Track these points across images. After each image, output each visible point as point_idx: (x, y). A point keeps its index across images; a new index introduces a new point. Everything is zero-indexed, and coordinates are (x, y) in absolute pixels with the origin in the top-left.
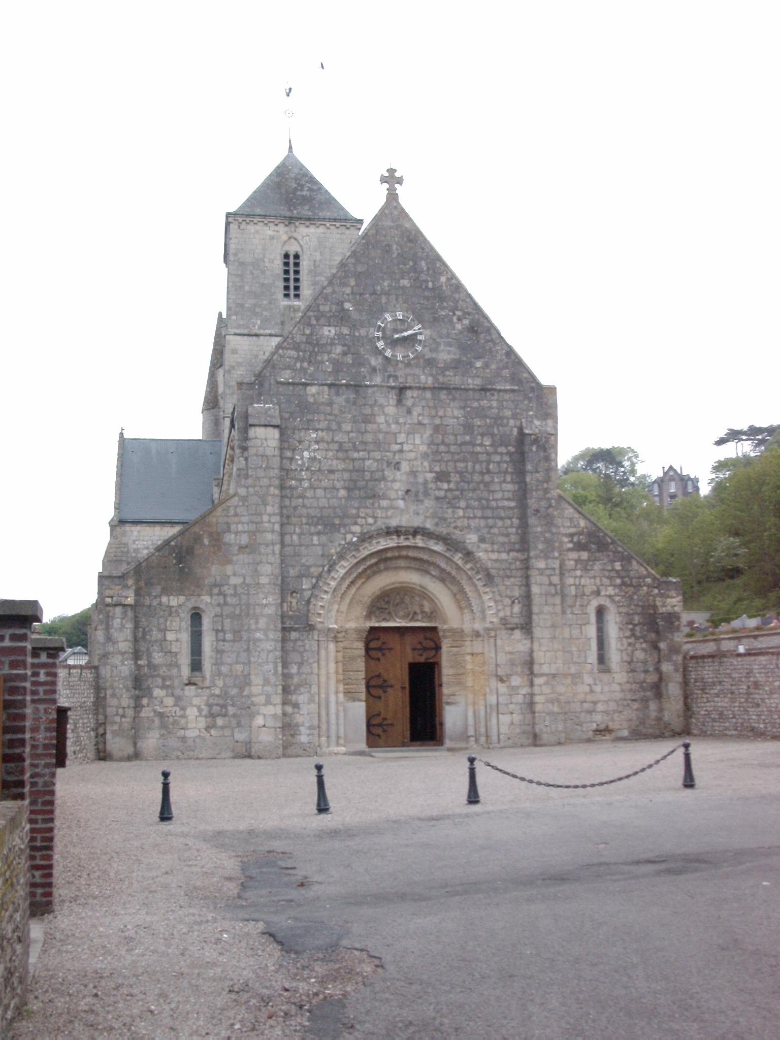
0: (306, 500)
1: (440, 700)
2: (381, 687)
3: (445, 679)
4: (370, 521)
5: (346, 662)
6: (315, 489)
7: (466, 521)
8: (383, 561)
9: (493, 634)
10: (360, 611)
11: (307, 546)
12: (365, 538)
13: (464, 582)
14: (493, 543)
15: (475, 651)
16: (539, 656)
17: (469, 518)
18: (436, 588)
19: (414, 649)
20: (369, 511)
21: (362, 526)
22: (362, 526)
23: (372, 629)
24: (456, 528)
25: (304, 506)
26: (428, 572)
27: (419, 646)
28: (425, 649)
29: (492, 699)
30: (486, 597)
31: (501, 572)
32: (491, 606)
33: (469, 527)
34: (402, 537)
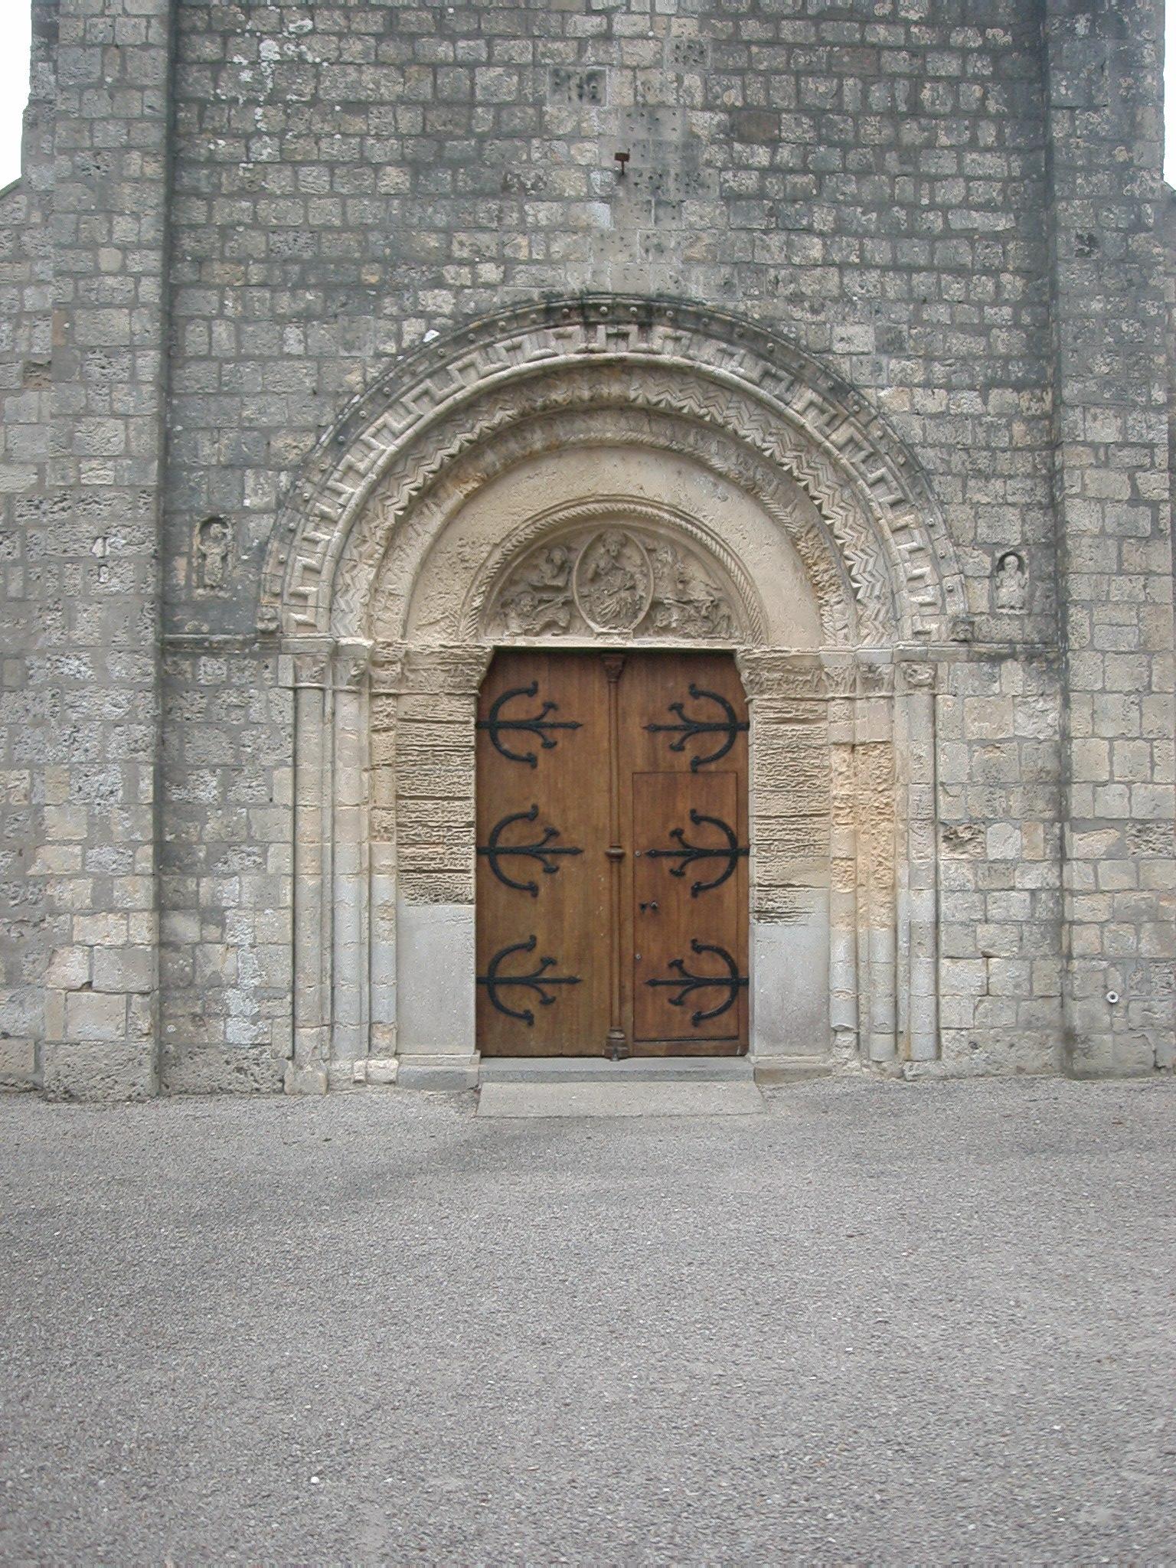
0: (263, 204)
2: (534, 853)
4: (490, 272)
8: (535, 417)
9: (924, 674)
10: (456, 590)
11: (263, 360)
12: (471, 332)
14: (929, 359)
16: (1090, 755)
17: (843, 267)
18: (748, 540)
19: (653, 729)
21: (458, 290)
22: (458, 290)
23: (502, 656)
24: (796, 299)
28: (693, 728)
29: (919, 906)
31: (957, 459)
32: (918, 579)
33: (844, 297)
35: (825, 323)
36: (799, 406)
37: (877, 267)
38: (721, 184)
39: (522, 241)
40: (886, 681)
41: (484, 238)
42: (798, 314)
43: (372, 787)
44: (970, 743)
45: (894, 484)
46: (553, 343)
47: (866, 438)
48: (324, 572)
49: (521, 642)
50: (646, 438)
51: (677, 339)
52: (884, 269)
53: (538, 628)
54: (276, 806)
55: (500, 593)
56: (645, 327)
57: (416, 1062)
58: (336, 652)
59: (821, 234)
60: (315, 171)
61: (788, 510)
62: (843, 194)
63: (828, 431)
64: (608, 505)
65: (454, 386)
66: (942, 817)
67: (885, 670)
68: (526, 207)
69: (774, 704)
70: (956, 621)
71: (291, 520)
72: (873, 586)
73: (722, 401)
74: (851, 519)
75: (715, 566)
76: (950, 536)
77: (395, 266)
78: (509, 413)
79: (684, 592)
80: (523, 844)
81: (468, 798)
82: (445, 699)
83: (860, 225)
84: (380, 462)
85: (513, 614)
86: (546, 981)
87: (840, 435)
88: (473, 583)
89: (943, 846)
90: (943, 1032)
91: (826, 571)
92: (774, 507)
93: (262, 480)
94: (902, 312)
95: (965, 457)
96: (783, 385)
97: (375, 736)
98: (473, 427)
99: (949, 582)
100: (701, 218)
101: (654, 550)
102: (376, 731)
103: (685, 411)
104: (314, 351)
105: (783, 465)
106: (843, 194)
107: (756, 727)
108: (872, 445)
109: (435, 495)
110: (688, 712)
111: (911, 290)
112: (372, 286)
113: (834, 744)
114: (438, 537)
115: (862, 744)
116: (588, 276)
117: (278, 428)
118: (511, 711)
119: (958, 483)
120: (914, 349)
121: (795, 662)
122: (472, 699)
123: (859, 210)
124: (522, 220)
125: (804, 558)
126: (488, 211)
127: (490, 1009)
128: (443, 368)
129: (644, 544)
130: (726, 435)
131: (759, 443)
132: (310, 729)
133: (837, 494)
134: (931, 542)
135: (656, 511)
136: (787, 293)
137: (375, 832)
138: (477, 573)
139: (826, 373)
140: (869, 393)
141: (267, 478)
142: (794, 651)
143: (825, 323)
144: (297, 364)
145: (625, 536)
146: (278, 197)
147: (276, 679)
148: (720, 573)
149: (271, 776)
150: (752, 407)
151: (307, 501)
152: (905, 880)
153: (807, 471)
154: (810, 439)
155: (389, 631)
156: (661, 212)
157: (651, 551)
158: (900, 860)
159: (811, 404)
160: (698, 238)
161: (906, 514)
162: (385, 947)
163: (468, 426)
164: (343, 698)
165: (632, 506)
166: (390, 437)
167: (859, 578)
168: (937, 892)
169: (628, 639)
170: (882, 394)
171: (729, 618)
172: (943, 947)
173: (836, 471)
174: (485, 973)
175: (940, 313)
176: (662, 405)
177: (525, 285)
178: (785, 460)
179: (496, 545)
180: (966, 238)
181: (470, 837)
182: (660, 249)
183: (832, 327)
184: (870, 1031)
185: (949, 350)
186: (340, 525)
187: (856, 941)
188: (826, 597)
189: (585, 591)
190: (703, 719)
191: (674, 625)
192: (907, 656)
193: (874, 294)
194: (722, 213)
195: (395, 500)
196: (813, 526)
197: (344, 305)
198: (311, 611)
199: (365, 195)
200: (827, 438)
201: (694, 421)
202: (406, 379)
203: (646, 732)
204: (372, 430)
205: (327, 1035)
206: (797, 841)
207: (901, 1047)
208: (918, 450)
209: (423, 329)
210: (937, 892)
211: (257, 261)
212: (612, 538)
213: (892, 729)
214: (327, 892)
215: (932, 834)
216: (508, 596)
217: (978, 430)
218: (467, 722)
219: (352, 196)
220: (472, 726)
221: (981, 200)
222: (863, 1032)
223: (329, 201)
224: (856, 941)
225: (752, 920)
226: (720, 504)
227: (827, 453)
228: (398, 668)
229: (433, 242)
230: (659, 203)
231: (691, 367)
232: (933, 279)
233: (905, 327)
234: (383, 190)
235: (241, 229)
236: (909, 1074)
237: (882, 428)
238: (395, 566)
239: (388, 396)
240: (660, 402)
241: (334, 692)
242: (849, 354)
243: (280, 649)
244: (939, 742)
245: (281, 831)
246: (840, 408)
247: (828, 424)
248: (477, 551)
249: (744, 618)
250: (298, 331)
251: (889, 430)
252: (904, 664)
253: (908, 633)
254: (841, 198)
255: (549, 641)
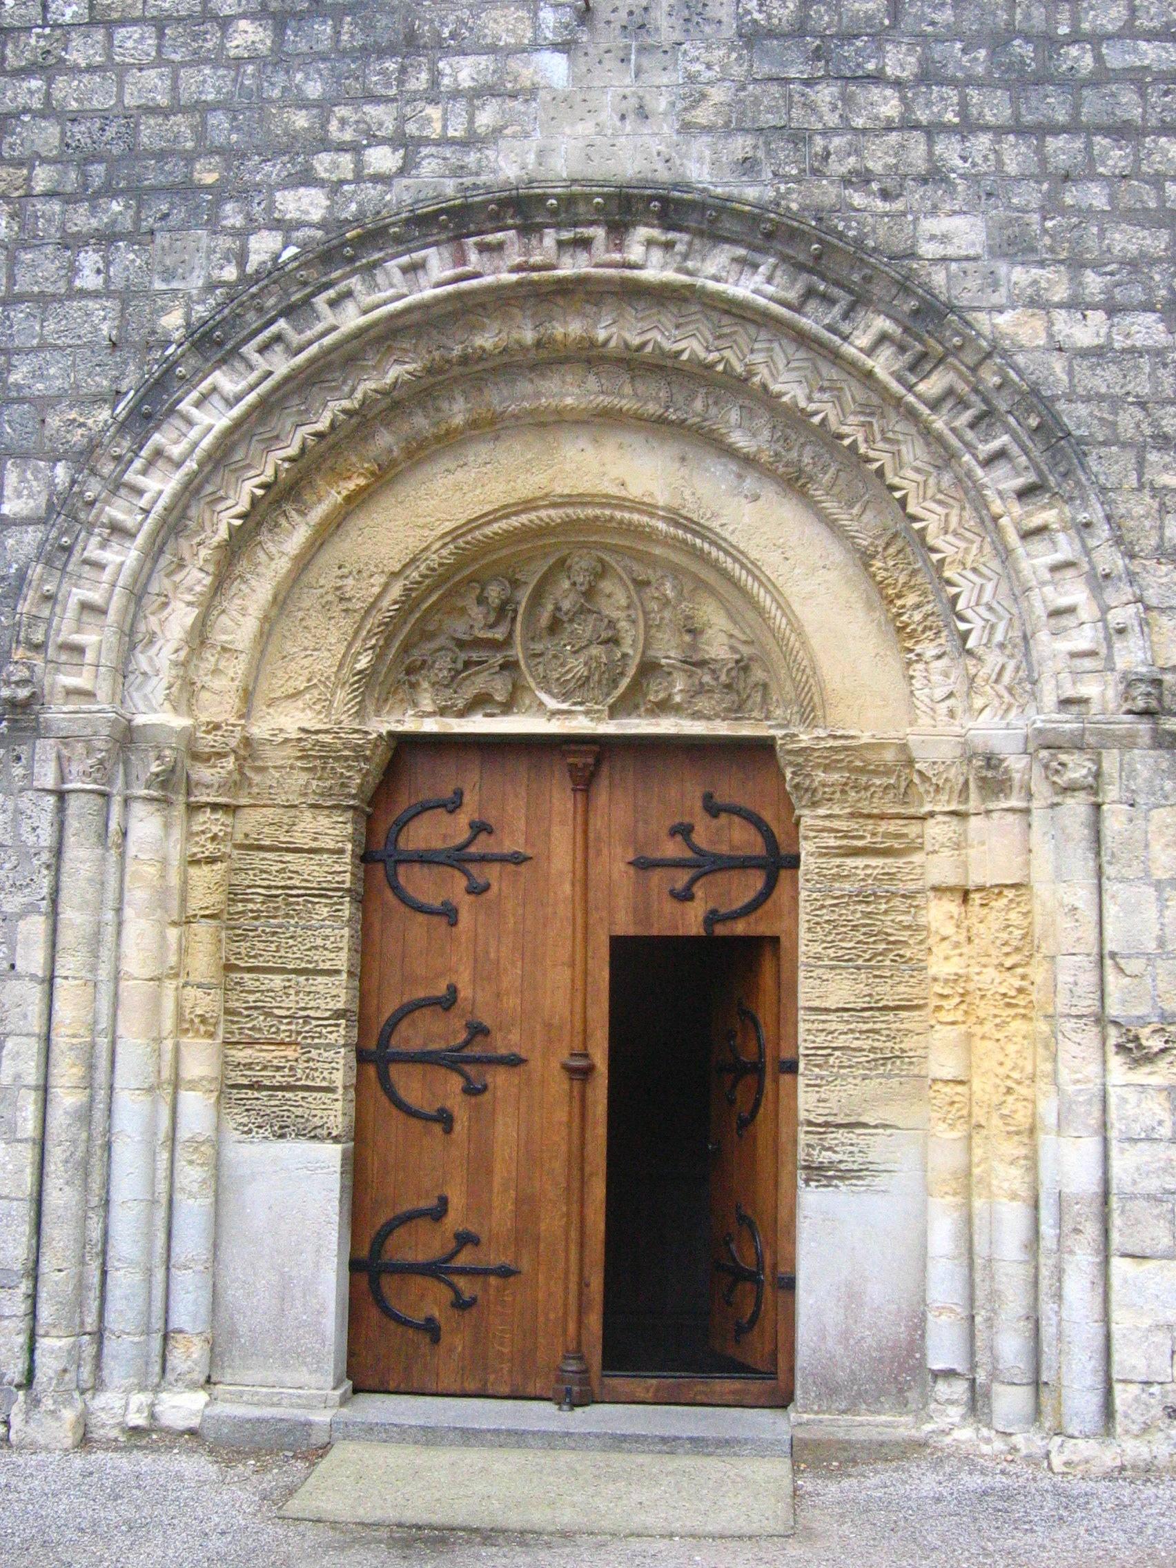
0: (61, 81)
1: (780, 1149)
2: (452, 1060)
3: (808, 1035)
4: (382, 159)
5: (242, 919)
6: (110, 26)
7: (917, 149)
8: (446, 381)
9: (1078, 768)
10: (325, 648)
11: (43, 300)
13: (909, 467)
14: (1076, 265)
15: (976, 878)
17: (932, 131)
19: (643, 865)
20: (382, 116)
21: (335, 188)
22: (335, 188)
23: (405, 747)
24: (861, 179)
25: (49, 111)
26: (712, 442)
27: (672, 849)
28: (708, 865)
29: (1072, 1164)
30: (1034, 560)
31: (1128, 420)
33: (935, 175)
34: (550, 238)
35: (904, 214)
36: (864, 341)
37: (986, 128)
38: (739, 17)
39: (434, 112)
40: (1016, 784)
41: (374, 112)
42: (858, 199)
43: (183, 951)
44: (1158, 885)
45: (1023, 460)
46: (473, 257)
47: (976, 391)
48: (112, 612)
49: (431, 726)
50: (625, 404)
51: (668, 246)
52: (999, 131)
53: (461, 704)
54: (19, 977)
55: (406, 649)
56: (618, 229)
57: (238, 1398)
58: (127, 738)
59: (898, 84)
60: (136, 32)
61: (855, 511)
62: (933, 23)
63: (913, 379)
64: (570, 511)
65: (319, 327)
66: (1113, 1010)
67: (1016, 764)
68: (441, 65)
69: (836, 824)
70: (1130, 682)
71: (62, 533)
72: (993, 627)
73: (742, 339)
74: (954, 521)
75: (740, 603)
76: (1118, 541)
77: (243, 156)
78: (406, 366)
79: (694, 647)
80: (432, 1047)
81: (338, 972)
82: (308, 815)
83: (962, 68)
84: (205, 443)
85: (425, 685)
86: (462, 1271)
87: (932, 385)
88: (356, 633)
89: (1116, 1061)
90: (1118, 1388)
91: (918, 606)
92: (831, 506)
93: (29, 476)
94: (1029, 195)
95: (1140, 415)
96: (837, 311)
97: (194, 871)
98: (353, 390)
99: (1117, 617)
100: (709, 66)
101: (647, 583)
102: (195, 862)
103: (685, 357)
104: (118, 284)
105: (841, 437)
106: (933, 23)
107: (807, 862)
108: (986, 400)
109: (298, 498)
110: (700, 838)
111: (1043, 161)
112: (208, 188)
113: (935, 889)
114: (305, 561)
115: (980, 889)
116: (531, 158)
117: (59, 398)
118: (426, 834)
119: (1130, 457)
120: (1051, 250)
121: (869, 755)
122: (350, 814)
123: (958, 45)
124: (434, 83)
125: (881, 586)
126: (383, 72)
127: (373, 1314)
128: (307, 301)
129: (630, 572)
130: (751, 395)
131: (802, 404)
132: (81, 857)
133: (932, 481)
134: (1087, 551)
135: (645, 519)
136: (843, 170)
137: (183, 1025)
138: (363, 619)
139: (904, 287)
140: (983, 321)
141: (36, 471)
142: (865, 738)
143: (904, 214)
144: (91, 304)
145: (601, 560)
146: (81, 71)
147: (29, 776)
148: (751, 615)
149: (14, 930)
150: (791, 348)
151: (91, 504)
152: (1052, 1120)
153: (880, 445)
154: (883, 390)
155: (219, 704)
156: (646, 62)
157: (641, 584)
158: (1043, 1085)
159: (883, 338)
160: (704, 96)
161: (1043, 508)
162: (193, 1212)
163: (346, 389)
164: (138, 809)
165: (608, 512)
166: (221, 405)
167: (969, 614)
168: (1106, 1141)
169: (599, 720)
170: (1000, 320)
171: (765, 686)
172: (1115, 1237)
173: (928, 444)
174: (364, 1253)
175: (1096, 196)
176: (649, 349)
177: (433, 180)
178: (845, 430)
179: (394, 575)
180: (1132, 81)
181: (339, 1034)
182: (643, 113)
183: (916, 219)
184: (994, 1375)
185: (1109, 250)
186: (140, 539)
187: (969, 1221)
188: (918, 649)
189: (538, 647)
190: (724, 849)
191: (678, 699)
192: (1051, 739)
193: (984, 168)
194: (740, 57)
195: (229, 503)
196: (895, 536)
197: (165, 217)
198: (87, 672)
199: (206, 61)
200: (910, 388)
201: (699, 376)
202: (251, 316)
203: (632, 870)
204: (194, 395)
205: (89, 1350)
206: (873, 1050)
207: (1047, 1408)
208: (1061, 406)
209: (279, 245)
210: (1106, 1141)
211: (45, 161)
212: (582, 563)
213: (1027, 863)
214: (98, 1115)
215: (1096, 1042)
216: (416, 655)
217: (1161, 372)
218: (341, 851)
219: (183, 64)
220: (347, 858)
221: (1155, 23)
222: (981, 1377)
223: (152, 73)
224: (969, 1221)
225: (801, 1183)
226: (748, 507)
227: (911, 414)
228: (230, 763)
229: (301, 120)
230: (642, 50)
231: (691, 287)
232: (1079, 144)
233: (1036, 217)
234: (232, 53)
235: (26, 118)
236: (1057, 1461)
237: (1001, 372)
238: (234, 606)
239: (220, 344)
240: (644, 344)
241: (127, 801)
242: (944, 259)
243: (38, 731)
244: (1106, 884)
245: (25, 1017)
246: (932, 342)
247: (912, 368)
248: (363, 584)
249: (788, 686)
250: (96, 257)
251: (1012, 374)
252: (1044, 754)
253: (1049, 698)
254: (930, 29)
255: (478, 724)
